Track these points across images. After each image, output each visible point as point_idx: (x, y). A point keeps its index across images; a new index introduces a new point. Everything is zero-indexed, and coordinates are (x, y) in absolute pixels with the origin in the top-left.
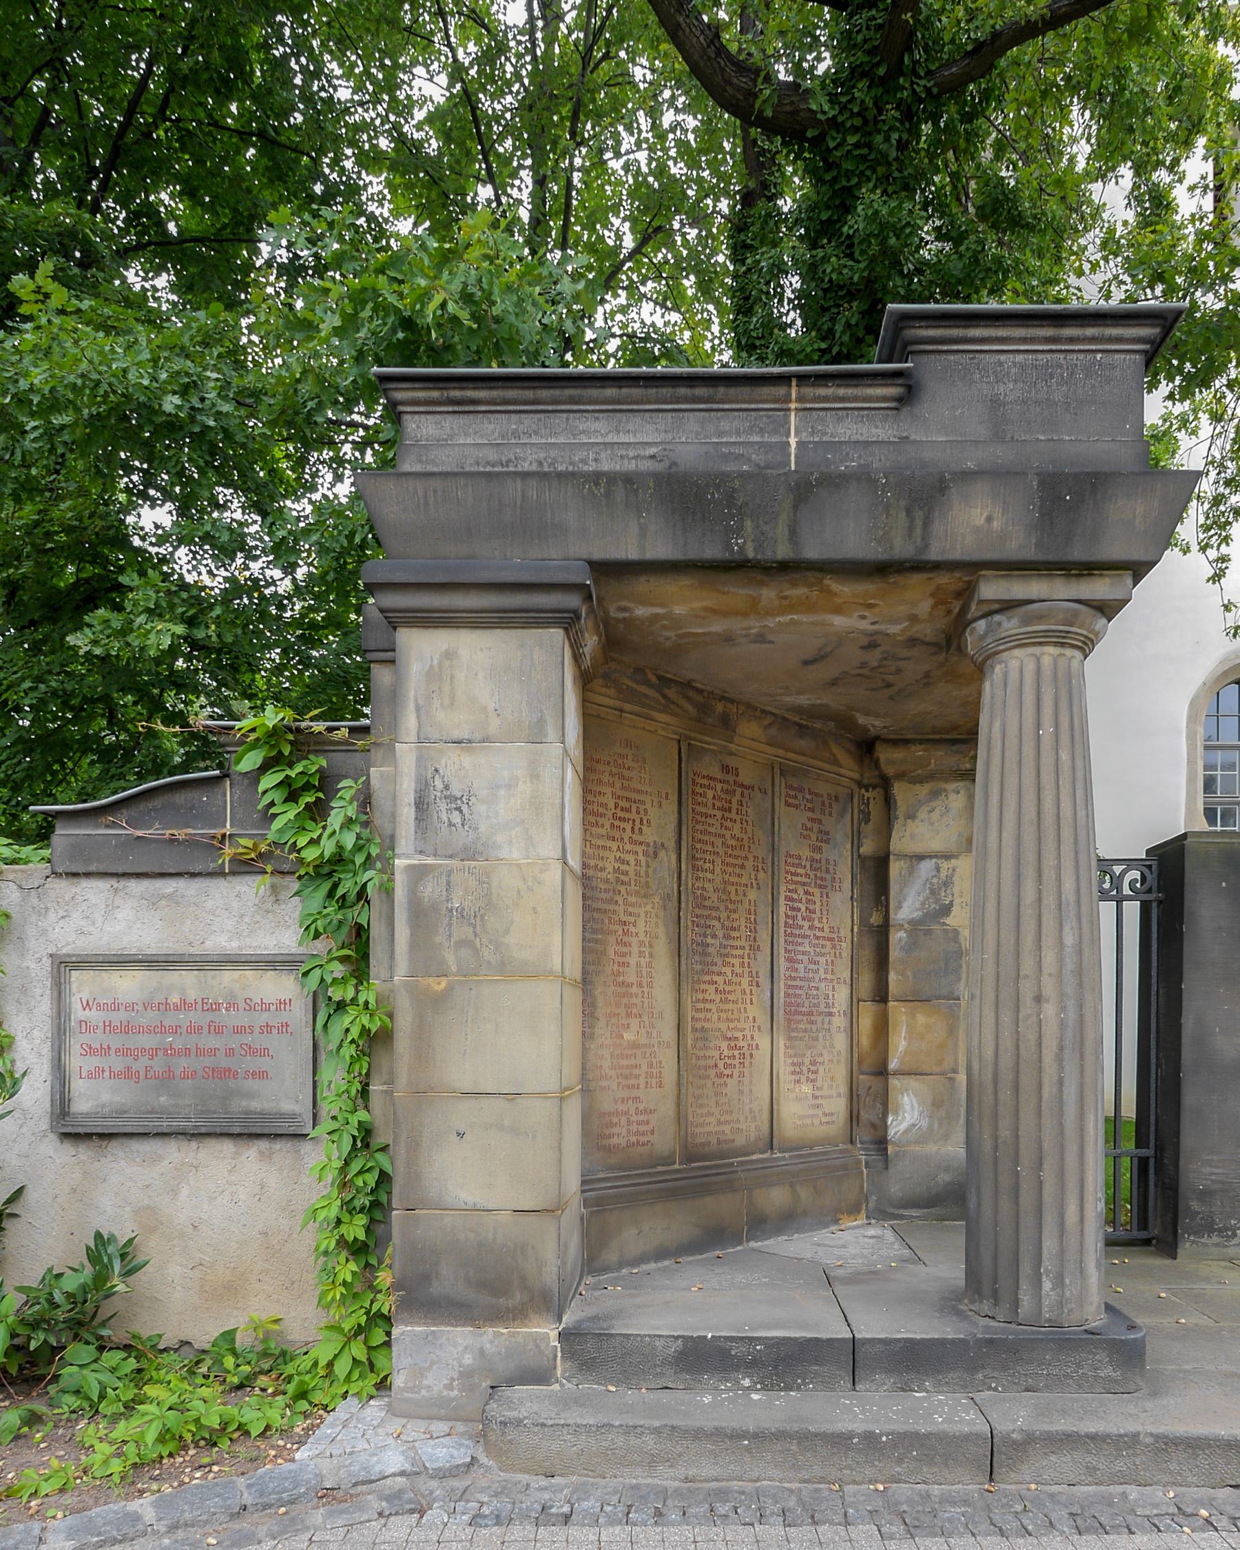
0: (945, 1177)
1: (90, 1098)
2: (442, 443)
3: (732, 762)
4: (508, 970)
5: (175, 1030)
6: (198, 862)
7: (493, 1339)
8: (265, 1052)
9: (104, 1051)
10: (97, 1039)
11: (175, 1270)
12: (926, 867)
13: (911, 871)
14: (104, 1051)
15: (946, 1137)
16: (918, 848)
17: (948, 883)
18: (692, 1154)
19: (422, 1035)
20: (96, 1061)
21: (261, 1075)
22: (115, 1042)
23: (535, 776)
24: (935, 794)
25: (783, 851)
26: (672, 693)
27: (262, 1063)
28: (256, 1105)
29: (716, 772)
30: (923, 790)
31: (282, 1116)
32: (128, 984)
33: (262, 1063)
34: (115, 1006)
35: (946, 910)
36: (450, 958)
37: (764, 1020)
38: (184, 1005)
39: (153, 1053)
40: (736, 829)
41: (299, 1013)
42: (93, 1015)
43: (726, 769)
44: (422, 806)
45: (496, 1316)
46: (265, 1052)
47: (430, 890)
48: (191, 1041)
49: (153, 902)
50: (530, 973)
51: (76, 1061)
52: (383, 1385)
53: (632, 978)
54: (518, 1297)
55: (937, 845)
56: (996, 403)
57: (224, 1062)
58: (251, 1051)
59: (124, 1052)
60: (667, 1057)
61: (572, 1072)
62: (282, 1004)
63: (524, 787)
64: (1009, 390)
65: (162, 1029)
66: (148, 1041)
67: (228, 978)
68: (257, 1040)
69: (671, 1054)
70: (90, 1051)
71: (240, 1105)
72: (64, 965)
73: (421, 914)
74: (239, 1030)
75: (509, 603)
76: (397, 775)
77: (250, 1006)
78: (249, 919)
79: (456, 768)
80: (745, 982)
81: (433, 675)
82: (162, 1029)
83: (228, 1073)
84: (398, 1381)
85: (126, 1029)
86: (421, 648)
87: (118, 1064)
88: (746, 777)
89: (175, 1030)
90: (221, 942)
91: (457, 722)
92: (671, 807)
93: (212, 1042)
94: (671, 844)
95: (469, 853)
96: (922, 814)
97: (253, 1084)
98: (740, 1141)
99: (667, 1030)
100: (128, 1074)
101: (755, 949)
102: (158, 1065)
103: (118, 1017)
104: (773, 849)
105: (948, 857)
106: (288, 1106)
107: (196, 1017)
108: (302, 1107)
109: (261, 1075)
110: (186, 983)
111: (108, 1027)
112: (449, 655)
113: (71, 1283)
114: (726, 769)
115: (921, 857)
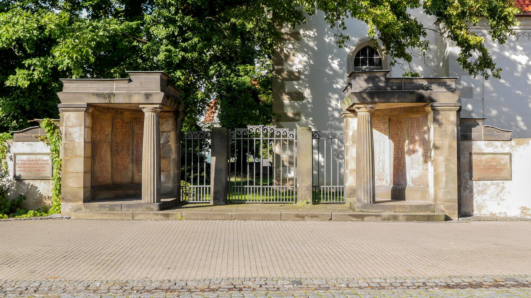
0: (168, 190)
2: (69, 87)
3: (123, 119)
5: (31, 164)
6: (36, 139)
7: (74, 204)
8: (45, 167)
9: (21, 167)
10: (20, 165)
11: (31, 200)
12: (165, 134)
13: (162, 135)
14: (21, 167)
15: (168, 183)
16: (164, 130)
17: (169, 137)
18: (114, 184)
19: (65, 165)
20: (20, 169)
21: (44, 171)
22: (23, 166)
23: (80, 131)
24: (167, 121)
25: (135, 132)
26: (110, 110)
27: (44, 169)
28: (43, 175)
29: (120, 121)
30: (164, 120)
31: (47, 177)
32: (25, 157)
33: (44, 169)
34: (23, 161)
35: (169, 141)
36: (69, 155)
37: (130, 162)
38: (33, 160)
39: (28, 167)
40: (124, 130)
41: (50, 161)
42: (20, 162)
43: (122, 120)
44: (65, 135)
45: (75, 201)
46: (45, 167)
47: (67, 146)
48: (34, 166)
49: (28, 145)
50: (79, 157)
51: (17, 169)
52: (60, 212)
53: (103, 155)
54: (78, 199)
55: (167, 130)
56: (141, 82)
57: (38, 169)
58: (43, 167)
59: (24, 167)
60: (110, 169)
61: (90, 169)
62: (47, 160)
63: (79, 132)
64: (143, 80)
65: (30, 164)
66: (27, 166)
67: (39, 156)
68: (43, 165)
69: (110, 167)
70: (19, 167)
71: (41, 175)
73: (65, 149)
74: (41, 164)
75: (76, 109)
76: (63, 129)
77: (43, 160)
78: (41, 147)
79: (70, 130)
80: (126, 156)
81: (67, 118)
82: (30, 164)
83: (39, 170)
84: (62, 210)
85: (24, 164)
86: (66, 114)
87: (23, 169)
88: (126, 121)
89: (31, 164)
90: (38, 151)
91: (70, 124)
92: (110, 128)
93: (37, 166)
94: (110, 134)
95: (72, 141)
96: (164, 124)
97: (43, 172)
98: (125, 182)
100: (24, 171)
101: (128, 150)
102: (29, 169)
103: (23, 162)
104: (133, 132)
105: (169, 132)
106: (48, 175)
107: (34, 162)
108: (50, 175)
109: (44, 171)
110: (33, 157)
111: (21, 164)
112: (69, 115)
113: (17, 200)
114: (122, 120)
115: (164, 132)
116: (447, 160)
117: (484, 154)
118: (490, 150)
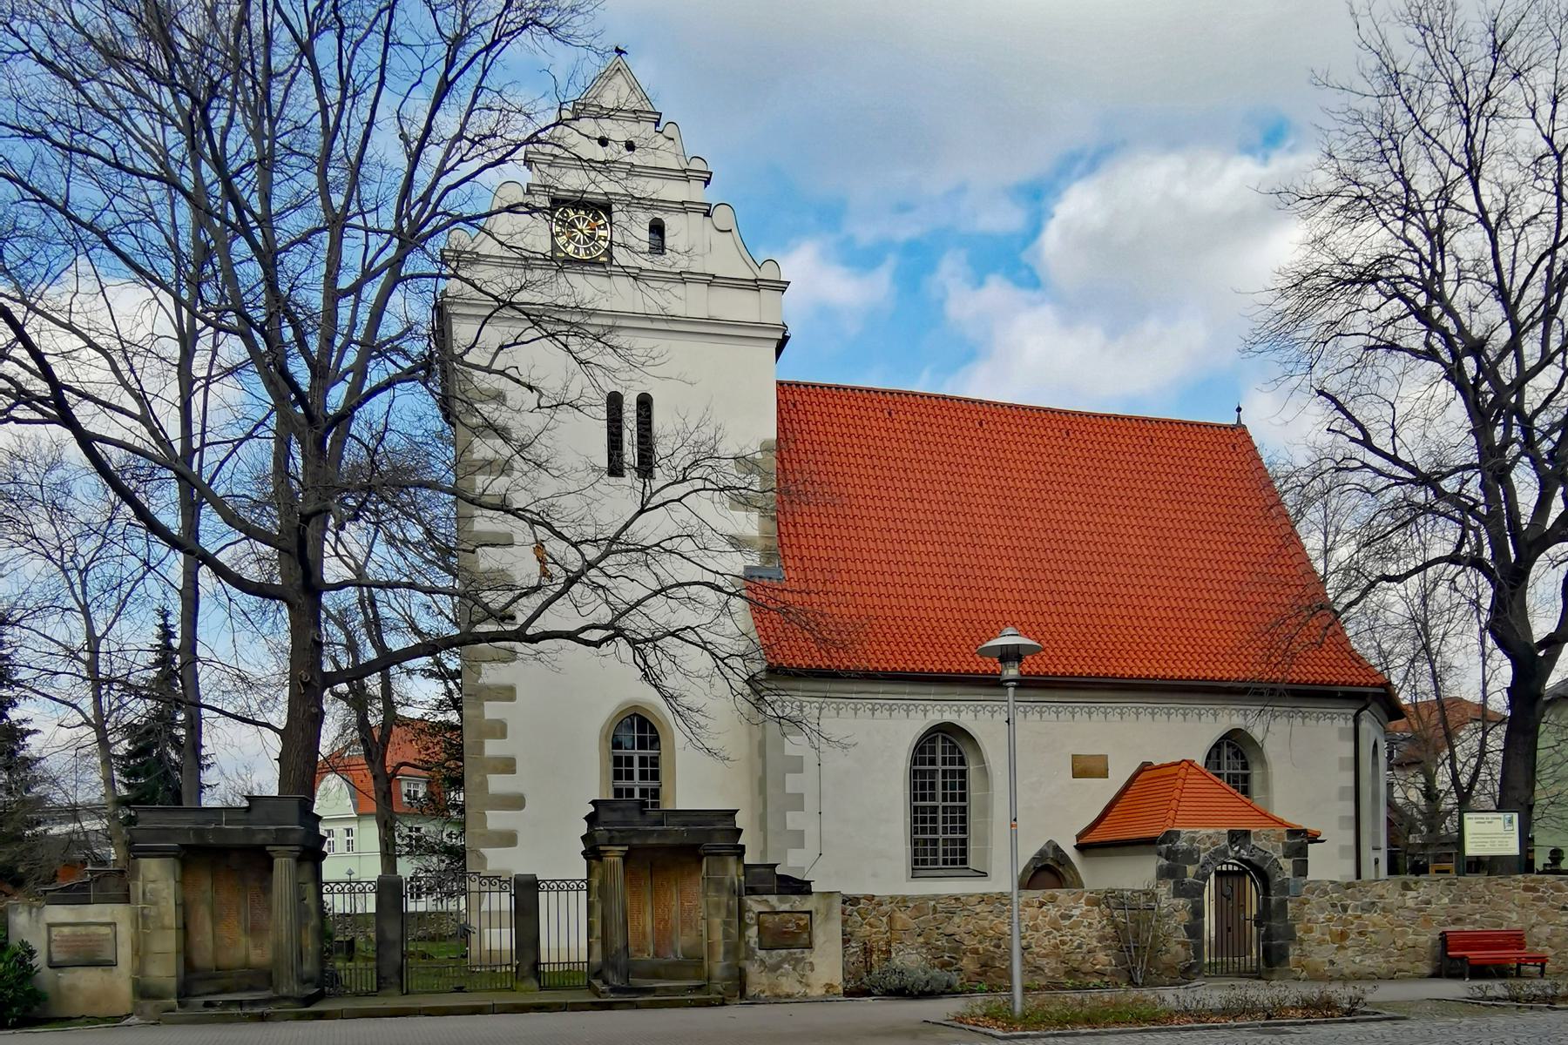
1: (57, 958)
4: (163, 928)
32: (66, 930)
67: (93, 929)
72: (50, 926)
99: (210, 936)
116: (726, 924)
117: (777, 913)
118: (786, 907)
